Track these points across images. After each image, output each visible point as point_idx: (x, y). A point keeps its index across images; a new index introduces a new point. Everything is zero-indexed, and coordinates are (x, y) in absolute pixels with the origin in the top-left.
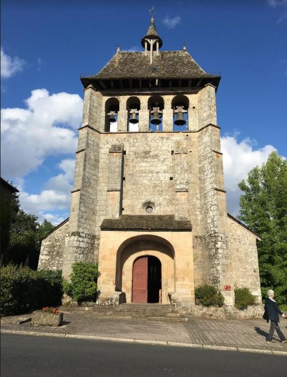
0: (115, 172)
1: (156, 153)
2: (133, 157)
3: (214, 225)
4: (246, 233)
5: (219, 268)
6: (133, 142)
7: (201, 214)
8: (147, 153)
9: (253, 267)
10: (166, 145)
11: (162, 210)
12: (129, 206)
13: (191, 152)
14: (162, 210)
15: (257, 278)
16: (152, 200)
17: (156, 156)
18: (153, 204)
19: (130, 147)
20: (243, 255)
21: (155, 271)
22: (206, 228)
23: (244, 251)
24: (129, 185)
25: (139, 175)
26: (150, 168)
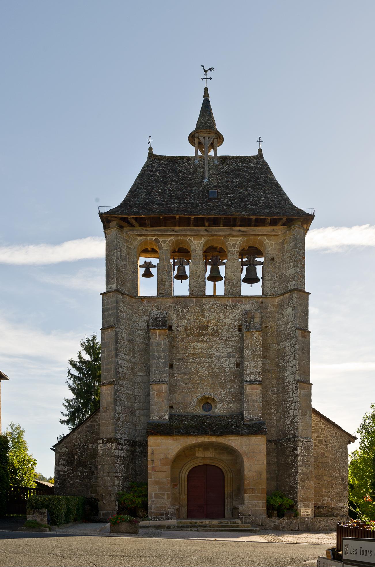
0: (160, 358)
2: (183, 334)
3: (293, 427)
4: (336, 433)
5: (298, 477)
6: (183, 311)
7: (277, 413)
8: (204, 328)
10: (230, 316)
11: (224, 407)
12: (179, 403)
13: (267, 327)
14: (224, 407)
16: (212, 395)
17: (217, 332)
18: (213, 400)
19: (178, 319)
20: (330, 461)
23: (331, 456)
26: (209, 351)
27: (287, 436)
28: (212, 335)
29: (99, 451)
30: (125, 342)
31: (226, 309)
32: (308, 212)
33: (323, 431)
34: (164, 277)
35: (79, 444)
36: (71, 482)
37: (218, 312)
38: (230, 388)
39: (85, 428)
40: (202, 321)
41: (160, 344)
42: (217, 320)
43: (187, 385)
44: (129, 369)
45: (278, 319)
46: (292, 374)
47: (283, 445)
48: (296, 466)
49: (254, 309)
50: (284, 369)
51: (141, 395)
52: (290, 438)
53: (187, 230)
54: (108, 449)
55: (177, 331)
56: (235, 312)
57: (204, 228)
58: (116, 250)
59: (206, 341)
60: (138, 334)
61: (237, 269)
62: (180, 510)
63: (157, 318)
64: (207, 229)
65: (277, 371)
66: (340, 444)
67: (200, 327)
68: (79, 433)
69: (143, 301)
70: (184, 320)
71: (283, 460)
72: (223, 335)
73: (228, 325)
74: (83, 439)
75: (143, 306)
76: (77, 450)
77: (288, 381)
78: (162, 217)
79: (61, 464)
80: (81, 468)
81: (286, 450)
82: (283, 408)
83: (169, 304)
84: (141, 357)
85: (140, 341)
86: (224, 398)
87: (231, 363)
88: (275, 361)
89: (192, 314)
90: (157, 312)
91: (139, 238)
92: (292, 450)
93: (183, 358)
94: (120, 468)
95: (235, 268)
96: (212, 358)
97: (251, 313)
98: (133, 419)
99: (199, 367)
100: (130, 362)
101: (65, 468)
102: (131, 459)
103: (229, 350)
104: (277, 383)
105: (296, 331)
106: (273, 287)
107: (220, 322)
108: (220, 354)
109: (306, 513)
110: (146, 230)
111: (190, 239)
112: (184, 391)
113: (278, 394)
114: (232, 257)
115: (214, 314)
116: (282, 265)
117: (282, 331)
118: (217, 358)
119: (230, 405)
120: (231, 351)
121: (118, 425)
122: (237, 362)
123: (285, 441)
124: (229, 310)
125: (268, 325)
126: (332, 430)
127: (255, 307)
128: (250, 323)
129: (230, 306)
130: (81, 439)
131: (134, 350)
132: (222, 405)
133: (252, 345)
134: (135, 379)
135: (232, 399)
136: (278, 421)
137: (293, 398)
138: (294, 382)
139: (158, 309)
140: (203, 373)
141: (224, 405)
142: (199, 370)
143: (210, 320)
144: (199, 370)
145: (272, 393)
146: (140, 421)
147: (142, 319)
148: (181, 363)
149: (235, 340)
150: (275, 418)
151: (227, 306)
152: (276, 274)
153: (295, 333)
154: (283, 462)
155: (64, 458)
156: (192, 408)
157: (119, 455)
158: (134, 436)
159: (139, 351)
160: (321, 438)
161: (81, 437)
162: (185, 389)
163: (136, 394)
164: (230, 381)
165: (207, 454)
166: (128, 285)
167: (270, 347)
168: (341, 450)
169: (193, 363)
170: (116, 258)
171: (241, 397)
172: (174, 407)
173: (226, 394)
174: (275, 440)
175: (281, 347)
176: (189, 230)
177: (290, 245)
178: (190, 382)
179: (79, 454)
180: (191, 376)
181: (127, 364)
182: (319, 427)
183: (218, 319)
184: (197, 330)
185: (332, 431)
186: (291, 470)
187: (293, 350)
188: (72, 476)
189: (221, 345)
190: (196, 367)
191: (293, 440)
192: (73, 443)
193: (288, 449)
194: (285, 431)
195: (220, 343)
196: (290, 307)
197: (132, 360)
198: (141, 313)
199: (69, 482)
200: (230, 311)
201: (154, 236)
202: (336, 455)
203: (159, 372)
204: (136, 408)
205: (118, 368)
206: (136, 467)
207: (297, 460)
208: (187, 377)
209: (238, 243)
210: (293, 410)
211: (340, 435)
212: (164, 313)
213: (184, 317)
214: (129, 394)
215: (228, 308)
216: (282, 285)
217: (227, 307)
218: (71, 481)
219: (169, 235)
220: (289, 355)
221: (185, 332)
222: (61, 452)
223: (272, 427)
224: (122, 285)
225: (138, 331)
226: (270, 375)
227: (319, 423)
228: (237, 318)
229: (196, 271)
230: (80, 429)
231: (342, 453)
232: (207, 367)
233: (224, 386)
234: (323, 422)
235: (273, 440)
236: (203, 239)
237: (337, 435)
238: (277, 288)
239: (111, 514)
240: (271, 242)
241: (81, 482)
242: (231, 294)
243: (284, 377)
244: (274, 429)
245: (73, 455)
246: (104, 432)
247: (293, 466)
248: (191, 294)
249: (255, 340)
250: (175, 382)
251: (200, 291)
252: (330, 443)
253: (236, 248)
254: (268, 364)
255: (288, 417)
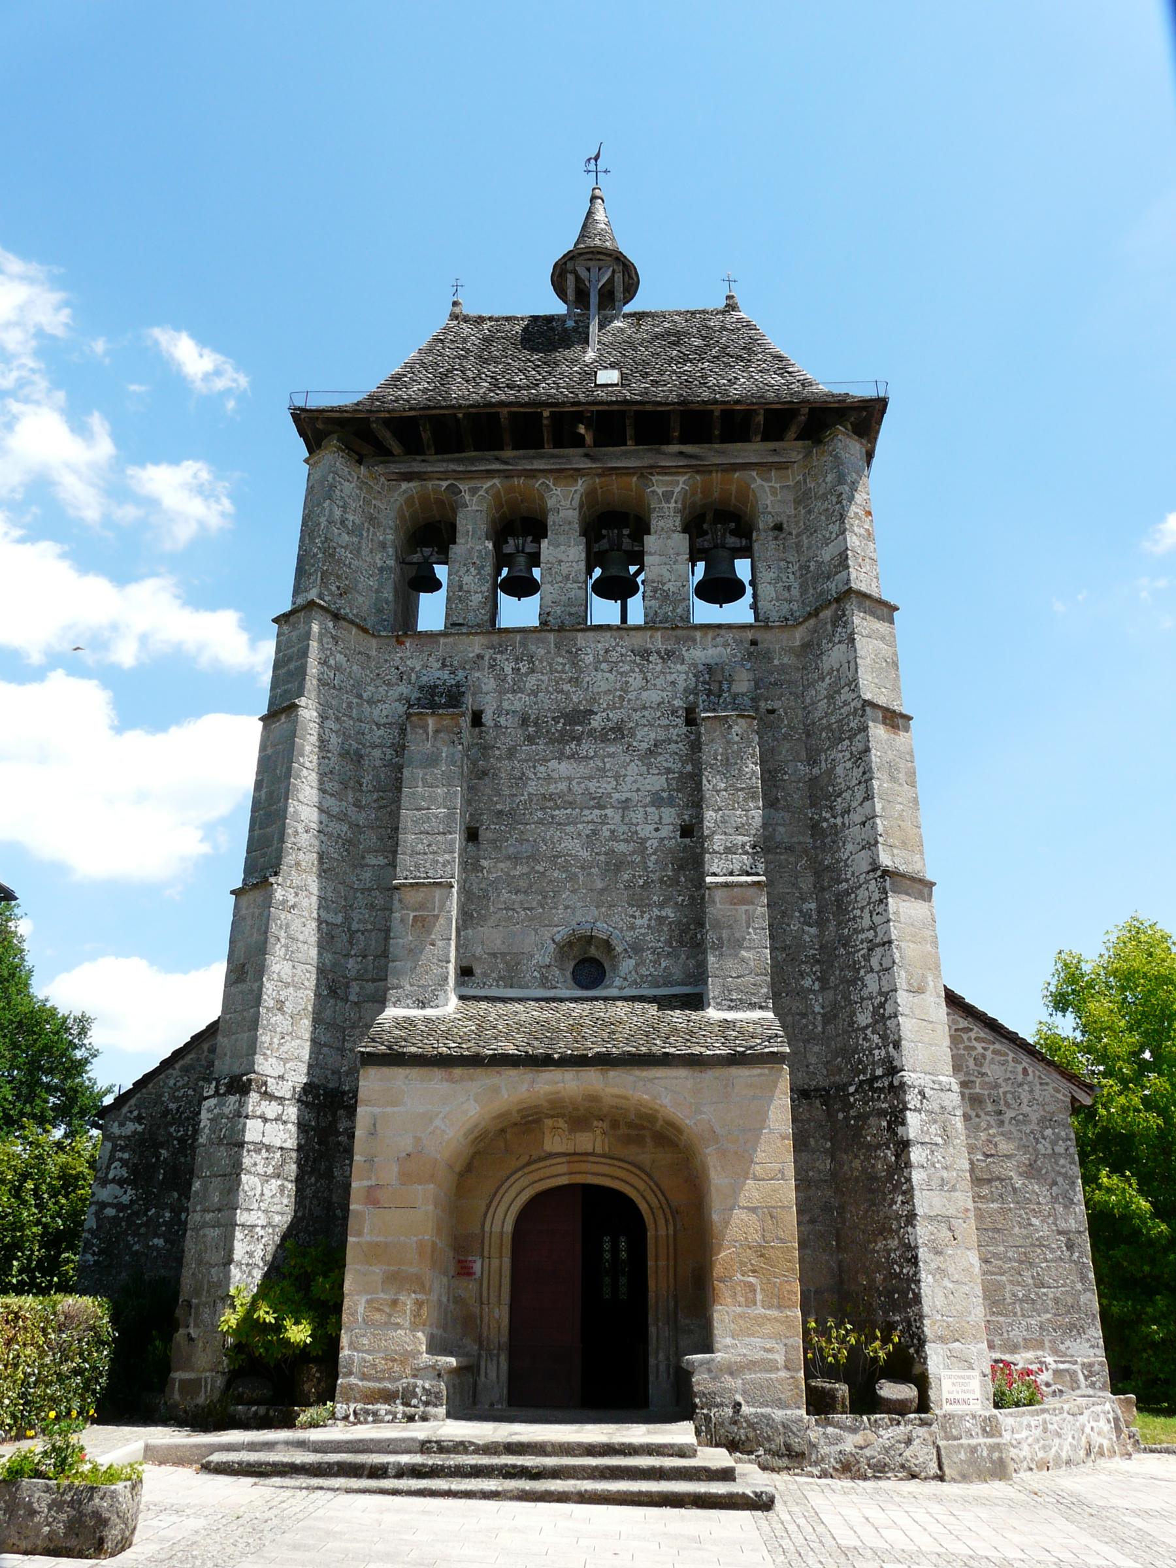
1: (615, 716)
2: (514, 733)
3: (884, 1037)
4: (1025, 1071)
6: (516, 670)
7: (823, 989)
8: (577, 717)
9: (1063, 1225)
10: (660, 682)
11: (644, 971)
12: (494, 955)
13: (772, 712)
15: (1083, 1278)
16: (602, 929)
18: (607, 946)
19: (501, 692)
21: (624, 1255)
22: (847, 1052)
24: (498, 860)
25: (540, 814)
26: (592, 785)
27: (864, 1072)
28: (603, 737)
29: (202, 1125)
30: (329, 755)
31: (648, 660)
32: (868, 392)
33: (981, 1065)
34: (466, 579)
35: (180, 1106)
36: (136, 1247)
37: (622, 670)
38: (661, 906)
39: (206, 1053)
40: (575, 699)
41: (436, 760)
42: (618, 693)
43: (521, 897)
44: (337, 843)
45: (806, 688)
46: (863, 848)
47: (852, 1106)
48: (904, 1187)
49: (730, 661)
50: (837, 836)
51: (371, 931)
52: (875, 1078)
53: (534, 458)
54: (228, 1118)
55: (497, 726)
56: (672, 671)
57: (581, 451)
58: (328, 501)
59: (586, 757)
60: (379, 738)
61: (678, 554)
62: (479, 1370)
63: (436, 686)
64: (592, 454)
65: (815, 848)
66: (1044, 1110)
67: (567, 715)
68: (187, 1071)
69: (402, 643)
70: (520, 695)
71: (857, 1163)
72: (639, 737)
73: (651, 707)
74: (194, 1090)
75: (401, 658)
76: (172, 1130)
77: (853, 872)
78: (460, 415)
79: (113, 1181)
80: (176, 1195)
81: (865, 1123)
82: (841, 970)
83: (477, 651)
84: (381, 807)
85: (381, 759)
86: (644, 940)
87: (664, 821)
88: (806, 815)
89: (545, 678)
90: (439, 674)
91: (404, 486)
92: (884, 1124)
93: (513, 809)
94: (262, 1194)
95: (672, 551)
96: (601, 807)
97: (723, 670)
98: (335, 1012)
99: (561, 838)
100: (343, 820)
101: (125, 1192)
102: (314, 1161)
103: (657, 782)
104: (815, 887)
105: (864, 710)
106: (786, 600)
107: (629, 700)
108: (628, 795)
109: (964, 1392)
110: (423, 461)
111: (543, 483)
112: (512, 917)
113: (821, 923)
114: (661, 523)
115: (611, 677)
116: (808, 537)
117: (820, 719)
118: (618, 808)
119: (663, 965)
120: (665, 786)
121: (275, 1025)
122: (684, 820)
123: (856, 1090)
124: (656, 664)
125: (777, 704)
126: (1010, 1058)
127: (735, 656)
128: (720, 696)
129: (658, 653)
130: (191, 1092)
131: (361, 785)
132: (637, 965)
133: (727, 759)
134: (358, 875)
135: (669, 943)
136: (828, 1019)
137: (876, 932)
138: (871, 875)
139: (444, 665)
140: (575, 857)
141: (643, 963)
142: (563, 845)
143: (598, 693)
144: (563, 845)
145: (802, 919)
146: (360, 1018)
147: (394, 693)
148: (506, 826)
149: (676, 753)
150: (817, 1009)
151: (648, 652)
152: (790, 565)
153: (862, 716)
154: (856, 1174)
155: (126, 1156)
156: (536, 974)
157: (266, 1141)
158: (333, 1073)
159: (377, 789)
160: (978, 1090)
161: (191, 1085)
162: (513, 909)
163: (355, 926)
164: (661, 881)
165: (585, 1141)
166: (361, 599)
167: (786, 773)
168: (1048, 1132)
169: (543, 824)
170: (327, 520)
171: (699, 936)
172: (478, 971)
173: (649, 926)
174: (824, 1089)
175: (820, 769)
176: (542, 457)
177: (824, 480)
178: (531, 887)
179: (175, 1142)
180: (537, 868)
181: (331, 824)
182: (966, 1048)
183: (622, 689)
184: (559, 722)
185: (1012, 1064)
186: (890, 1206)
187: (861, 770)
188: (141, 1225)
189: (633, 769)
190: (552, 837)
191: (886, 1083)
192: (163, 1102)
193: (872, 1120)
194: (855, 1051)
195: (628, 761)
196: (840, 642)
197: (349, 813)
198: (393, 676)
199: (128, 1246)
200: (659, 668)
201: (446, 479)
202: (1035, 1150)
203: (429, 845)
204: (352, 974)
205: (296, 831)
206: (331, 1191)
207: (908, 1164)
208: (524, 871)
209: (677, 490)
210: (878, 972)
211: (1040, 1077)
212: (461, 674)
213: (519, 688)
214: (328, 924)
215: (651, 658)
216: (811, 591)
217: (649, 656)
218: (135, 1243)
219: (488, 471)
220: (848, 788)
221: (520, 731)
222: (120, 1137)
223: (808, 1041)
224: (341, 594)
225: (379, 729)
226: (792, 859)
227: (965, 1037)
228: (681, 685)
229: (560, 561)
230: (190, 1057)
231: (1054, 1143)
232: (587, 836)
233: (642, 900)
234: (978, 1031)
235: (816, 1090)
236: (580, 482)
237: (1030, 1078)
238: (797, 601)
239: (206, 1387)
240: (772, 484)
241: (168, 1246)
242: (661, 622)
243: (838, 862)
244: (816, 1049)
245: (157, 1146)
246: (225, 1055)
247: (896, 1188)
248: (544, 623)
249: (737, 743)
250: (483, 886)
251: (570, 614)
252: (1007, 1105)
253: (673, 500)
254: (784, 825)
255: (862, 999)
